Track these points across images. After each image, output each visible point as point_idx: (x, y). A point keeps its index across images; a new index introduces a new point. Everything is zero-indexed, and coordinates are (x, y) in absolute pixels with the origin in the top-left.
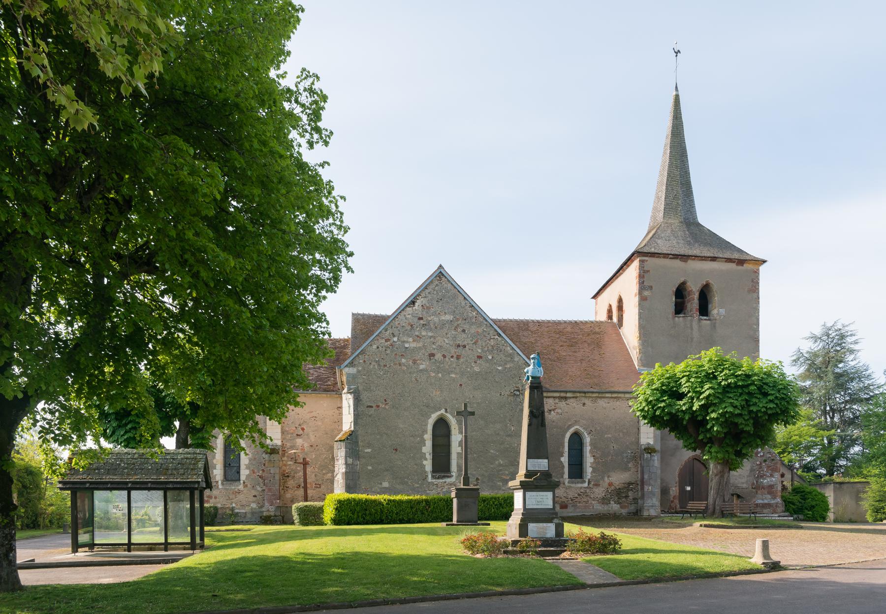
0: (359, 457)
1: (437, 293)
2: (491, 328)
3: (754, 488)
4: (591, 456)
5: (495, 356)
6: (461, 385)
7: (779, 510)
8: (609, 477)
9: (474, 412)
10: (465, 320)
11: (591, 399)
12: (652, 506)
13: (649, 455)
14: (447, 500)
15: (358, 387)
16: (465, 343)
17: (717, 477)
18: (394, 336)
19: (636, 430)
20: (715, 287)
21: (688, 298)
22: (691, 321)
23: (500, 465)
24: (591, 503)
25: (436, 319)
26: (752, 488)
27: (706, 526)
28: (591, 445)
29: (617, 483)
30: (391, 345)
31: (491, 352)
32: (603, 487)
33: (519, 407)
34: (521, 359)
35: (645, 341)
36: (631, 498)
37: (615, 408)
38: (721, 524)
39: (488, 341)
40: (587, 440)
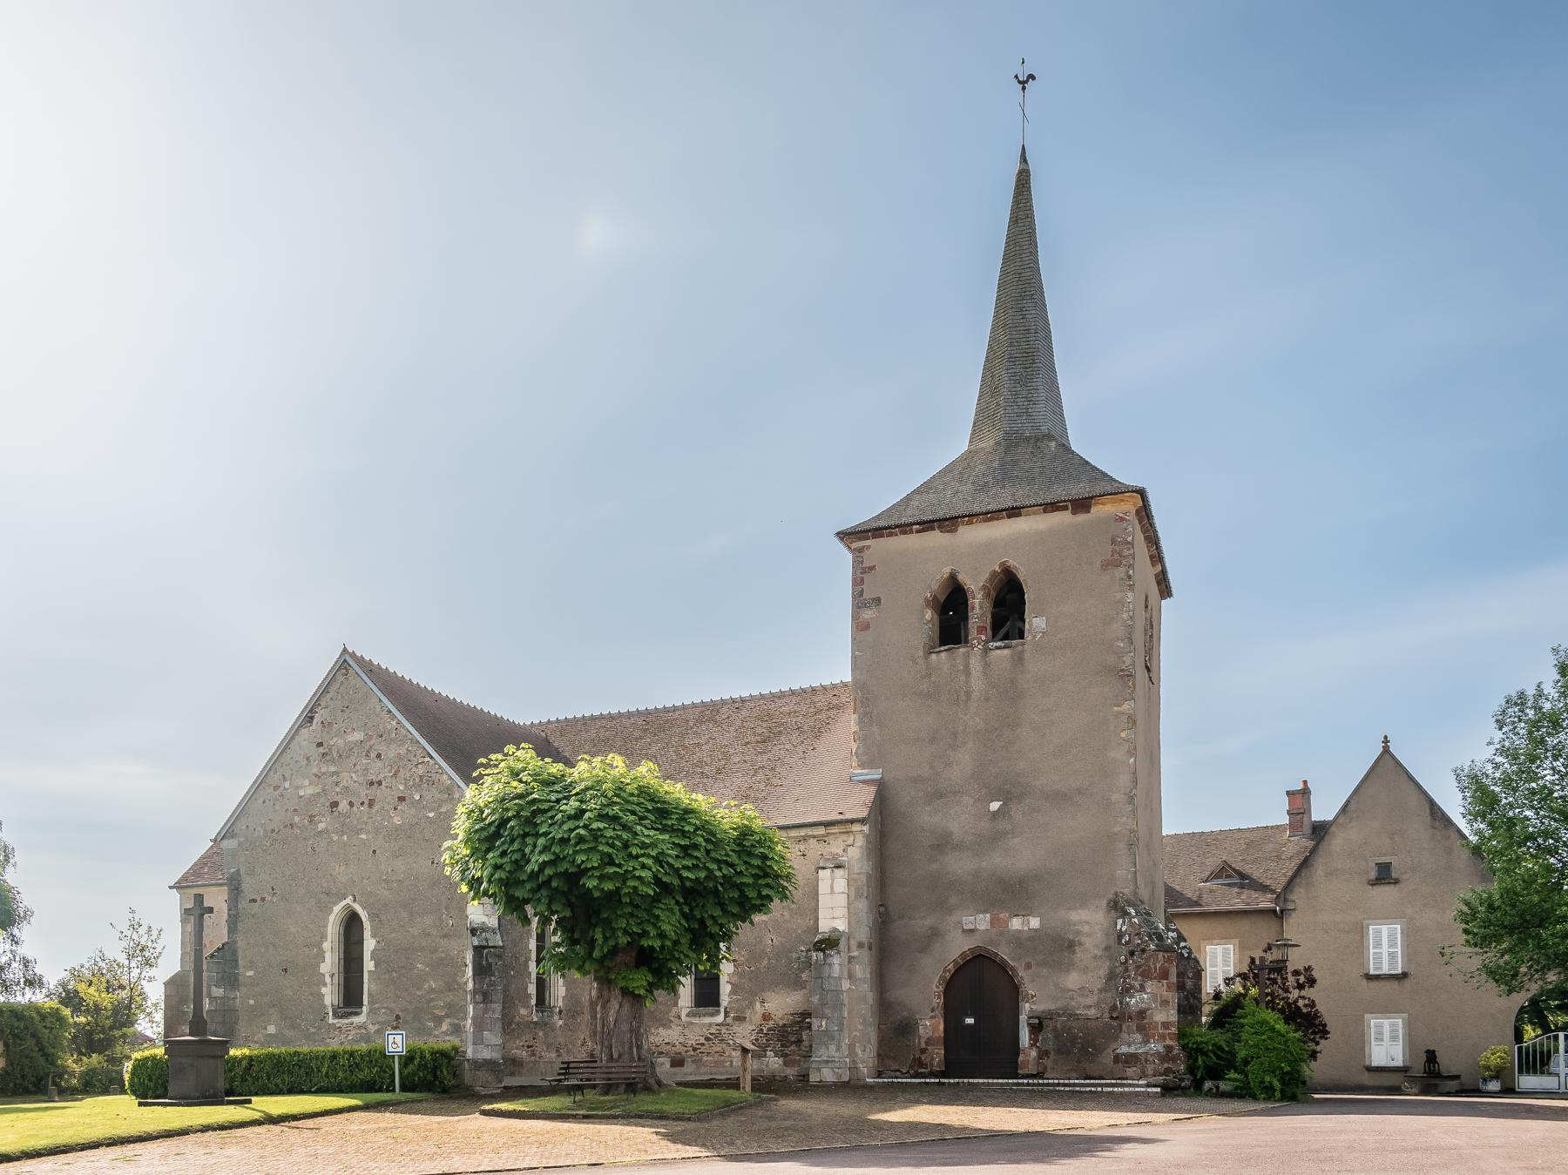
0: (238, 985)
1: (342, 697)
6: (374, 852)
7: (1150, 1069)
9: (212, 908)
10: (381, 736)
12: (827, 1062)
13: (821, 955)
15: (239, 870)
16: (381, 777)
18: (285, 780)
22: (967, 656)
23: (432, 990)
24: (729, 1056)
25: (341, 742)
26: (1112, 1018)
29: (780, 1014)
30: (282, 795)
31: (418, 787)
32: (751, 1024)
35: (866, 714)
39: (414, 769)
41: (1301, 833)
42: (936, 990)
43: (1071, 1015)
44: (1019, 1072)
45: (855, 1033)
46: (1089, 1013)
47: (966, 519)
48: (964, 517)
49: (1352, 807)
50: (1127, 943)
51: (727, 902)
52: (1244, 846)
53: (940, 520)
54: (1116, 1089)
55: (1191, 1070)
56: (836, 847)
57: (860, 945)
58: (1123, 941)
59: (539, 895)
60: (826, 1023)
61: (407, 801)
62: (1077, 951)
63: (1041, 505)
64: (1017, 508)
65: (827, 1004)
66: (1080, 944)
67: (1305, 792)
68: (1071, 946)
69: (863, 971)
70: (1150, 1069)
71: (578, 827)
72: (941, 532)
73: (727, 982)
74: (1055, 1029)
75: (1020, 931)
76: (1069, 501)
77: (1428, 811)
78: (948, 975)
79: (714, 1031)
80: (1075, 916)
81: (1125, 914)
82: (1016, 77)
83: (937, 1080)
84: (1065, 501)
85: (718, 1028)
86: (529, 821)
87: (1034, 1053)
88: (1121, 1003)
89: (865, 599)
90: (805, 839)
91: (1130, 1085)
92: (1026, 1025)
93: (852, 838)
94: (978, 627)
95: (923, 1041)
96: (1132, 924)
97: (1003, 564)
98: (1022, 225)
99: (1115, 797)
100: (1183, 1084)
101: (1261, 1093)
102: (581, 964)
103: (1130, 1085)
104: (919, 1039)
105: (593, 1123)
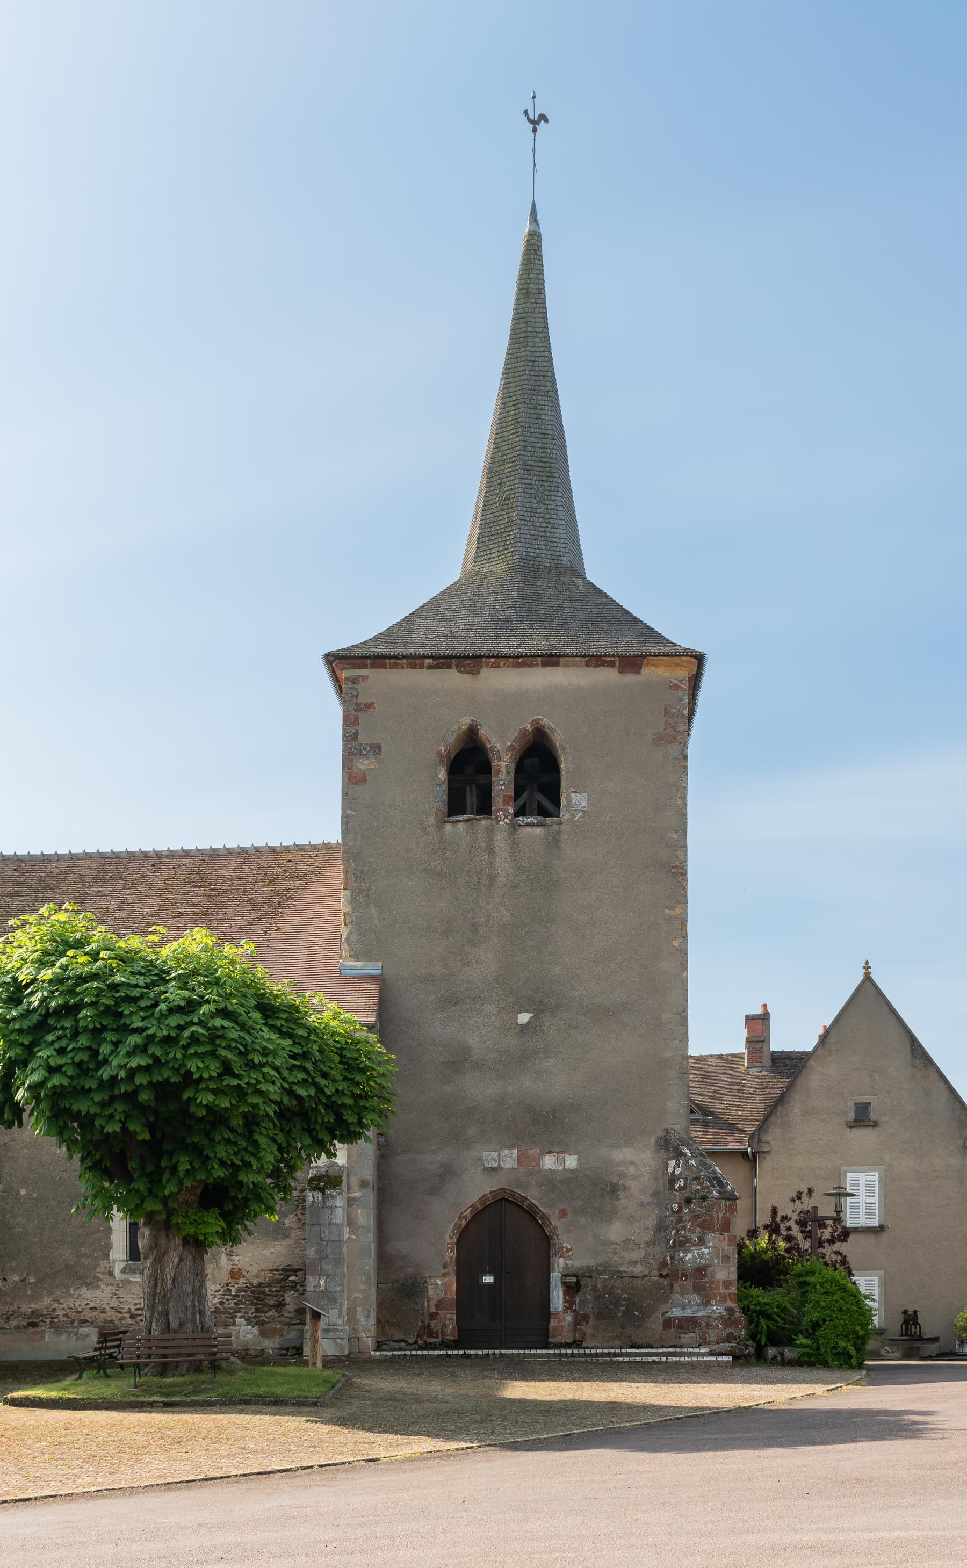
7: (712, 1335)
13: (319, 1195)
22: (490, 831)
26: (661, 1275)
29: (254, 1270)
35: (360, 891)
36: (290, 1308)
38: (67, 1395)
41: (760, 1064)
42: (449, 1241)
43: (613, 1273)
44: (551, 1340)
45: (355, 1295)
46: (634, 1270)
47: (493, 660)
48: (489, 657)
49: (831, 1039)
50: (681, 1188)
51: (318, 1128)
52: (700, 1077)
53: (460, 657)
54: (682, 1359)
55: (753, 1336)
57: (363, 1184)
58: (676, 1186)
59: (111, 1110)
60: (326, 1282)
62: (621, 1197)
64: (555, 656)
65: (327, 1257)
66: (625, 1189)
67: (765, 1017)
68: (614, 1190)
69: (365, 1217)
70: (712, 1335)
71: (192, 1023)
72: (460, 671)
74: (594, 1289)
76: (618, 656)
77: (909, 1048)
78: (464, 1222)
80: (621, 1155)
81: (679, 1154)
82: (526, 113)
83: (461, 1352)
84: (613, 656)
86: (113, 1012)
87: (569, 1318)
88: (672, 1258)
89: (361, 745)
91: (691, 1354)
92: (559, 1284)
94: (505, 796)
95: (433, 1304)
96: (688, 1167)
97: (535, 722)
98: (534, 300)
99: (665, 1017)
100: (747, 1352)
101: (833, 1360)
102: (138, 1201)
103: (691, 1354)
104: (428, 1301)
105: (179, 1412)
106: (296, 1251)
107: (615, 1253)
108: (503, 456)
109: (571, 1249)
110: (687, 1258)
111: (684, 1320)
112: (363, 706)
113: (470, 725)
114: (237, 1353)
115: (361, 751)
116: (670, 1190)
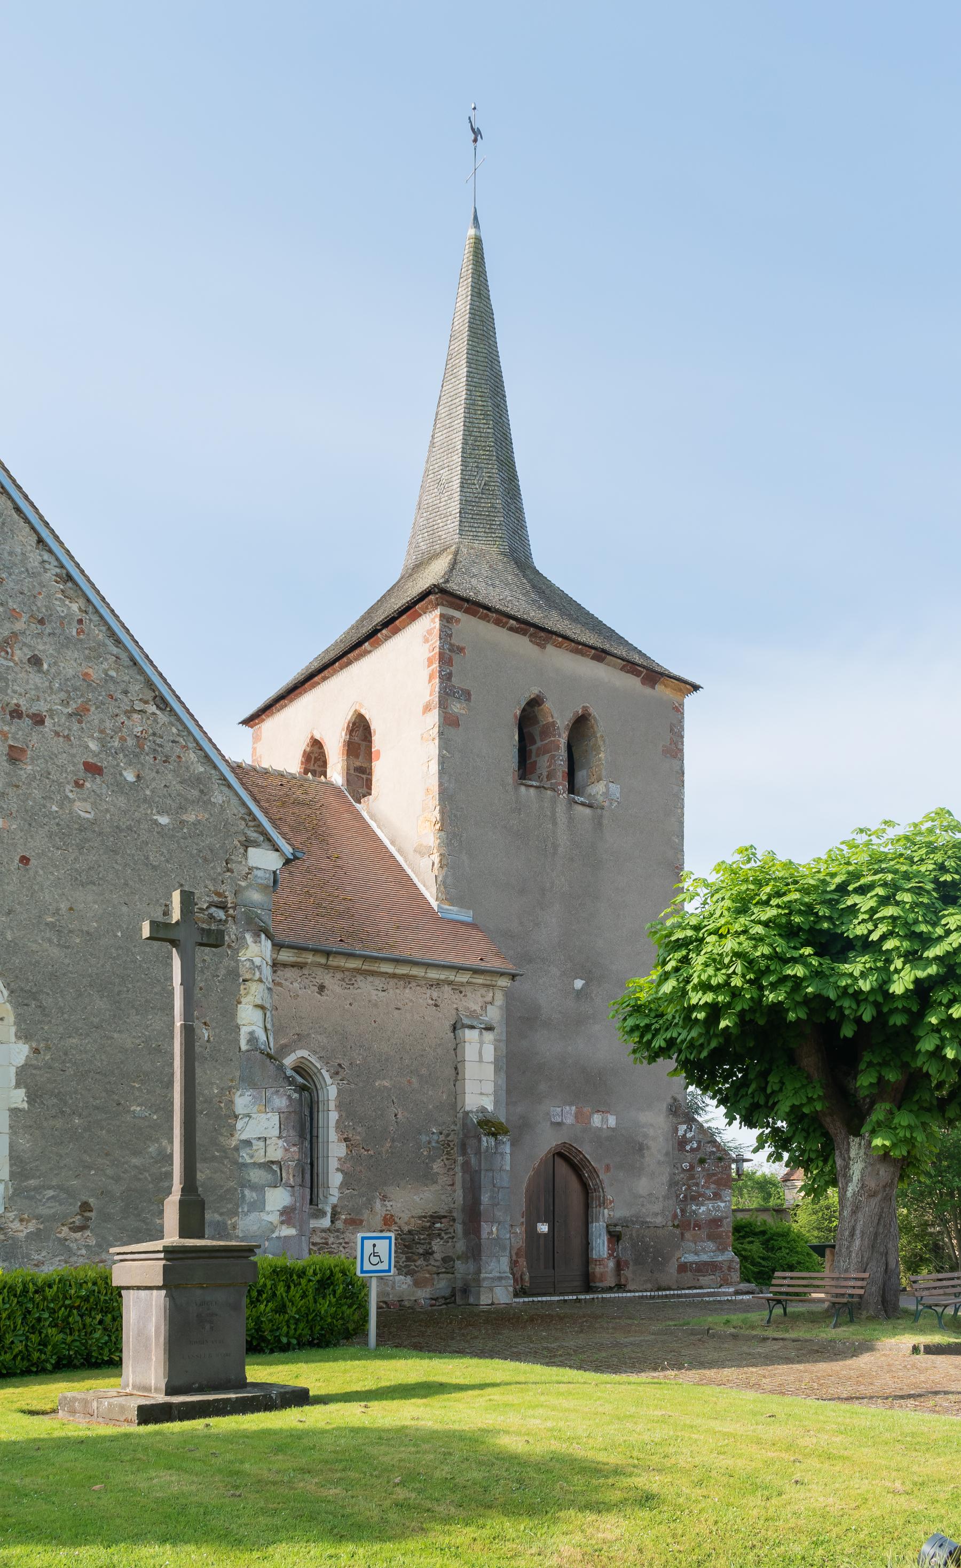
2: (133, 672)
3: (678, 1226)
4: (339, 1141)
5: (148, 774)
6: (25, 860)
8: (384, 1198)
10: (41, 622)
11: (339, 975)
13: (492, 1140)
14: (25, 1291)
16: (41, 707)
17: (874, 1202)
19: (449, 1071)
20: (602, 726)
21: (539, 744)
22: (554, 802)
26: (674, 1226)
27: (931, 1350)
28: (339, 1107)
29: (405, 1216)
31: (134, 757)
33: (226, 961)
34: (234, 801)
36: (438, 1256)
37: (400, 1005)
40: (331, 1091)
50: (692, 1150)
56: (473, 1002)
60: (497, 1229)
61: (108, 778)
62: (646, 1155)
63: (623, 659)
65: (498, 1204)
72: (531, 641)
73: (338, 1170)
74: (631, 1238)
75: (601, 1129)
79: (318, 1240)
83: (575, 1297)
85: (324, 1235)
88: (683, 1211)
89: (454, 687)
90: (438, 984)
93: (491, 994)
106: (443, 1197)
107: (643, 1205)
108: (476, 441)
109: (613, 1201)
110: (701, 1211)
111: (702, 1264)
112: (455, 649)
113: (538, 696)
114: (393, 1305)
115: (454, 693)
116: (679, 1150)
